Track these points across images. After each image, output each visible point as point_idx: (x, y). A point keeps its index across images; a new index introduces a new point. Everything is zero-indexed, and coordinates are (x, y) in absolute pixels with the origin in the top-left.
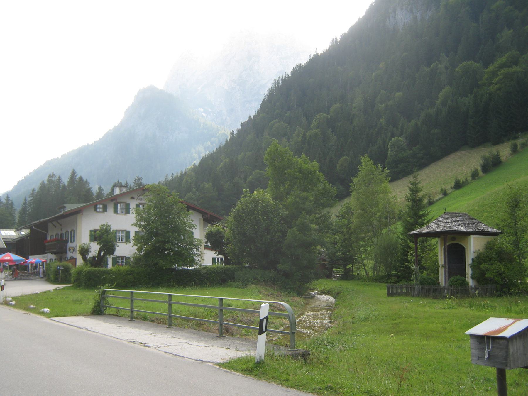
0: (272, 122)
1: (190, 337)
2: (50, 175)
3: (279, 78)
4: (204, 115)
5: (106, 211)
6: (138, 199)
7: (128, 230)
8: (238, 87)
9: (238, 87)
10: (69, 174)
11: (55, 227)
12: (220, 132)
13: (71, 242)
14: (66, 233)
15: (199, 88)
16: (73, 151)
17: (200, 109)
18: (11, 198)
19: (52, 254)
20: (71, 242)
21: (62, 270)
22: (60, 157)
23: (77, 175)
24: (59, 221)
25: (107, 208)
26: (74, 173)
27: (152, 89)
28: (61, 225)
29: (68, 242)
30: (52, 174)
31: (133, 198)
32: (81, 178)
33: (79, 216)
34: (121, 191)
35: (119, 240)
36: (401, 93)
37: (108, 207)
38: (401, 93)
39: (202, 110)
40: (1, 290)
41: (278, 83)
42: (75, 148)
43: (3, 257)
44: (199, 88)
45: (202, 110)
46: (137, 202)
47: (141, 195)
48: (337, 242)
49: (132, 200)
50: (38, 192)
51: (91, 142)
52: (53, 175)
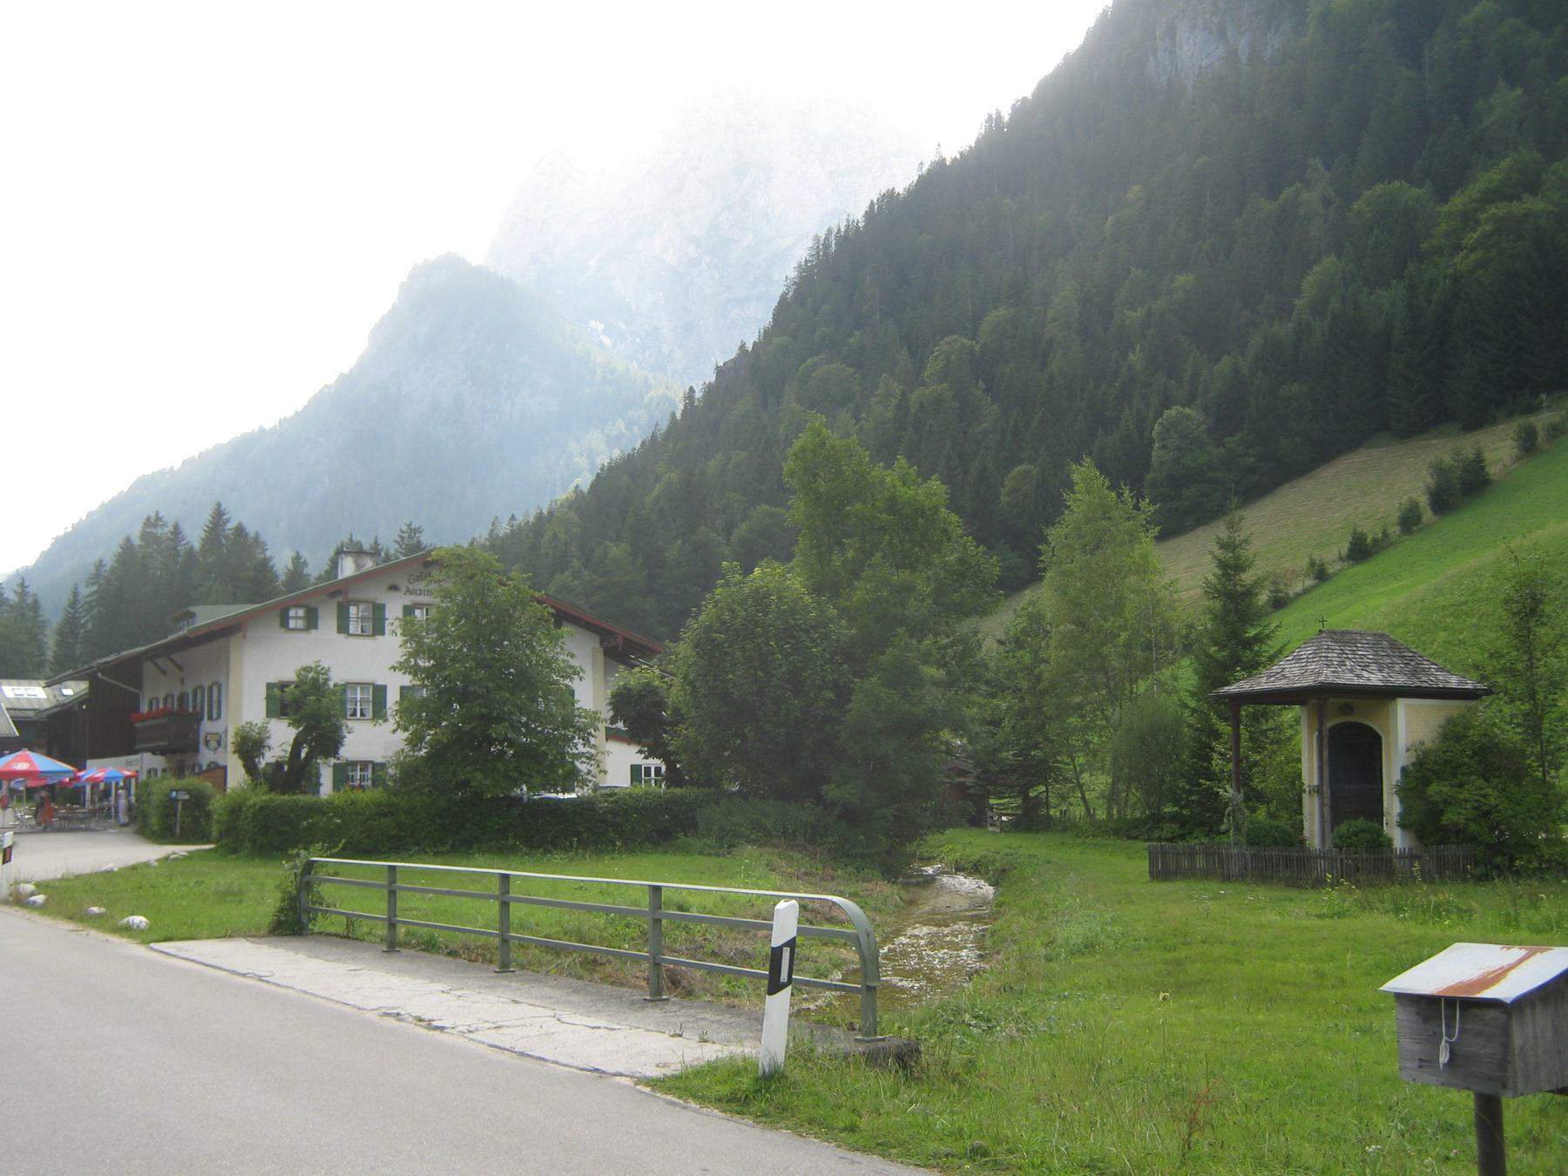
0: (809, 361)
1: (565, 1002)
2: (148, 519)
3: (830, 231)
4: (607, 341)
5: (316, 627)
6: (408, 591)
7: (380, 682)
8: (707, 259)
9: (707, 259)
10: (206, 517)
11: (164, 673)
12: (652, 393)
13: (210, 718)
14: (195, 692)
15: (592, 262)
16: (217, 448)
17: (593, 323)
18: (32, 589)
19: (154, 753)
20: (210, 718)
21: (184, 801)
22: (177, 466)
23: (228, 520)
24: (175, 656)
25: (316, 618)
26: (219, 515)
27: (451, 264)
28: (180, 668)
29: (202, 718)
30: (153, 516)
31: (394, 588)
32: (240, 530)
33: (234, 640)
34: (358, 566)
35: (354, 714)
36: (1192, 277)
37: (320, 614)
38: (1192, 277)
39: (600, 327)
40: (4, 862)
41: (826, 246)
42: (224, 439)
43: (8, 764)
44: (592, 262)
45: (600, 327)
46: (408, 600)
47: (420, 578)
48: (1002, 720)
49: (393, 594)
50: (113, 569)
51: (270, 422)
52: (158, 518)
